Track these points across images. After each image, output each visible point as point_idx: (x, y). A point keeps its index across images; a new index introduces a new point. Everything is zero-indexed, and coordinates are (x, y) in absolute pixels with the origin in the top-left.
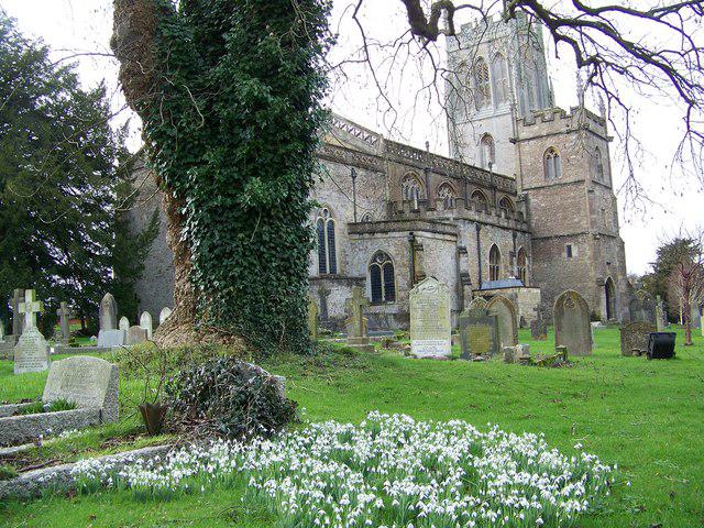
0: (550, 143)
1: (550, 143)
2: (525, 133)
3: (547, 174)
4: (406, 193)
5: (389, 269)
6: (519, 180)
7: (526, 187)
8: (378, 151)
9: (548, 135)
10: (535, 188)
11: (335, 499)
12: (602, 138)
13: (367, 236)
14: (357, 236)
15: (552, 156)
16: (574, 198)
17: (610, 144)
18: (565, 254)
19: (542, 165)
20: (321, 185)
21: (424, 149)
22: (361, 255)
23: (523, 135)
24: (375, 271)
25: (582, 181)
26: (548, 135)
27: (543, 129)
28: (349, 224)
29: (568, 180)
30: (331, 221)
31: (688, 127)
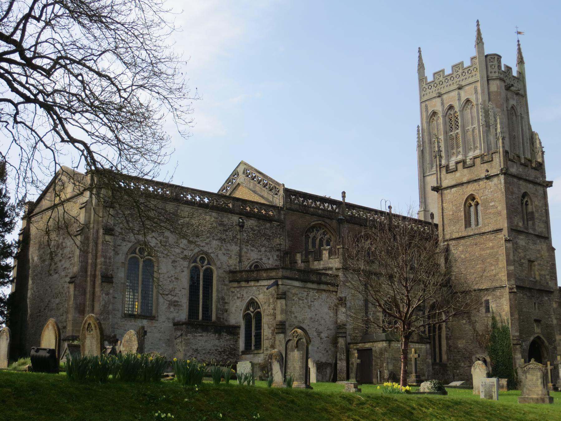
0: (469, 190)
1: (469, 190)
2: (448, 180)
3: (468, 224)
4: (33, 85)
5: (258, 316)
6: (440, 228)
7: (447, 237)
8: (279, 201)
9: (468, 182)
10: (458, 238)
11: (62, 322)
12: (539, 184)
13: (243, 284)
14: (236, 285)
15: (473, 204)
16: (492, 248)
17: (549, 190)
18: (483, 310)
19: (463, 214)
20: (321, 328)
21: (340, 199)
22: (238, 303)
23: (445, 184)
24: (247, 317)
25: (500, 230)
26: (468, 182)
27: (462, 175)
28: (231, 272)
29: (487, 229)
30: (207, 270)
31: (124, 63)
